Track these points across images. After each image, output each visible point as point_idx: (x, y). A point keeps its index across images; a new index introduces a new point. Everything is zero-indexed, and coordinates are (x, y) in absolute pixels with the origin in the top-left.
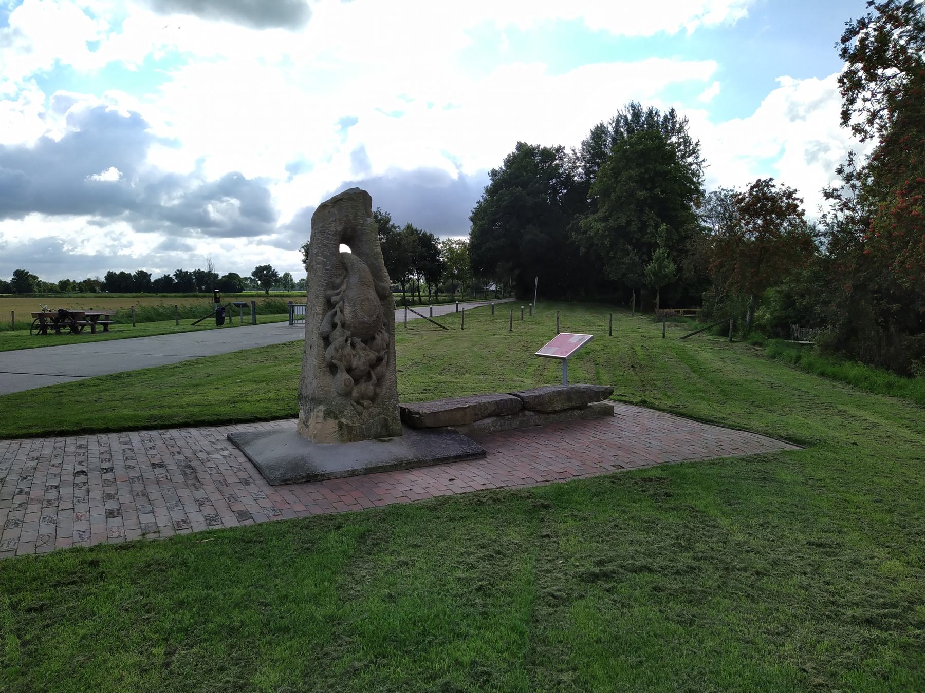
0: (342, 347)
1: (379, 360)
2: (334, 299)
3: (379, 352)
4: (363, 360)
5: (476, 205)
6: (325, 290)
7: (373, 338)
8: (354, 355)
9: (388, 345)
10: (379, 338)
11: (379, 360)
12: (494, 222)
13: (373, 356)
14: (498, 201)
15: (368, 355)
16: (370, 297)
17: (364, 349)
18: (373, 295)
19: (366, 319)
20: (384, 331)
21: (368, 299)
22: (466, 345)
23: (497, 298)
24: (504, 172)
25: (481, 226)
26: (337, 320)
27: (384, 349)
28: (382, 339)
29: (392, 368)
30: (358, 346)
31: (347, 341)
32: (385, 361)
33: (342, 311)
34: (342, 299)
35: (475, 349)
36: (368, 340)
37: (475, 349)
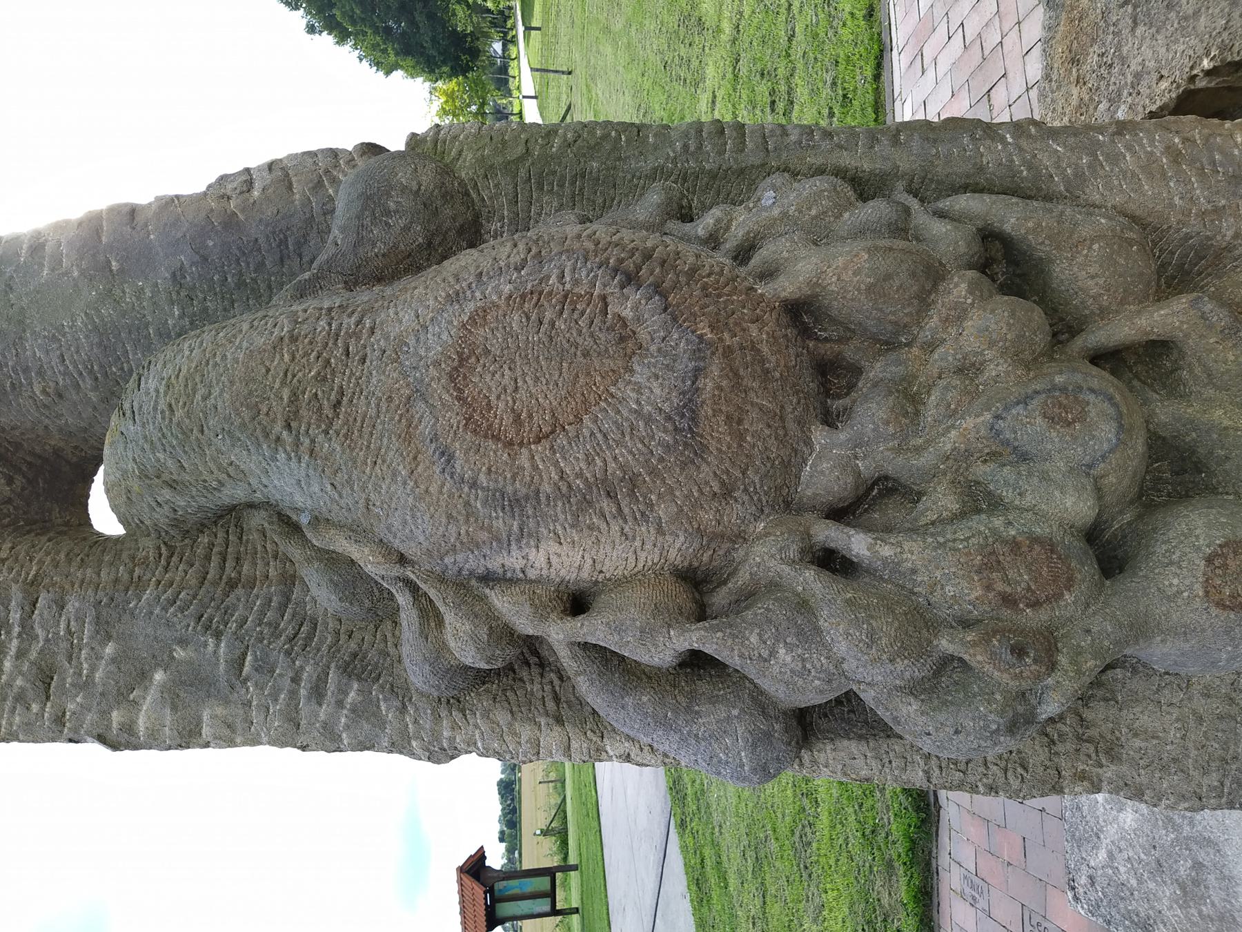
0: (918, 620)
1: (1006, 265)
2: (464, 643)
3: (933, 275)
4: (1030, 427)
5: (365, 63)
6: (401, 693)
7: (801, 314)
8: (978, 500)
9: (864, 187)
10: (801, 269)
11: (1006, 265)
12: (388, 30)
13: (980, 324)
14: (354, 23)
15: (967, 369)
16: (440, 339)
17: (909, 399)
18: (420, 316)
19: (649, 388)
20: (741, 223)
21: (460, 366)
22: (608, 50)
23: (514, 41)
24: (308, 13)
25: (397, 54)
26: (662, 651)
27: (900, 228)
28: (819, 236)
29: (1054, 160)
30: (881, 458)
31: (832, 562)
32: (1012, 217)
33: (577, 603)
34: (472, 588)
35: (618, 25)
36: (823, 359)
37: (618, 25)
